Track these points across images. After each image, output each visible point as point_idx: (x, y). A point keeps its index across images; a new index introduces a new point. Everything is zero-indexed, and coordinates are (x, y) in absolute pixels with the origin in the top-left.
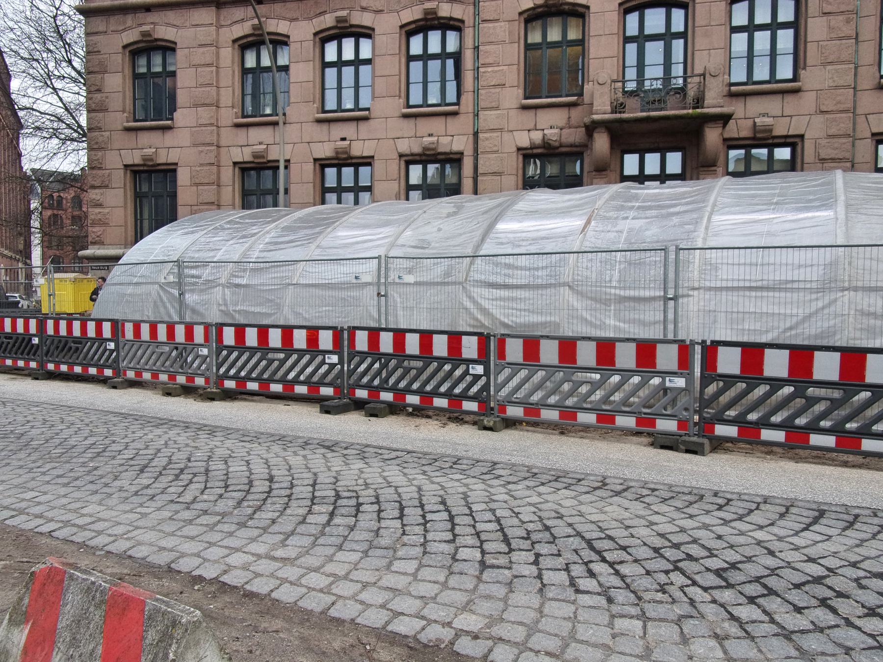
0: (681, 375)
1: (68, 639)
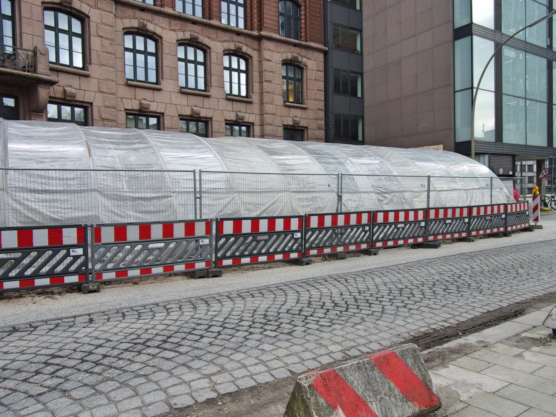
0: (207, 238)
1: (371, 394)
